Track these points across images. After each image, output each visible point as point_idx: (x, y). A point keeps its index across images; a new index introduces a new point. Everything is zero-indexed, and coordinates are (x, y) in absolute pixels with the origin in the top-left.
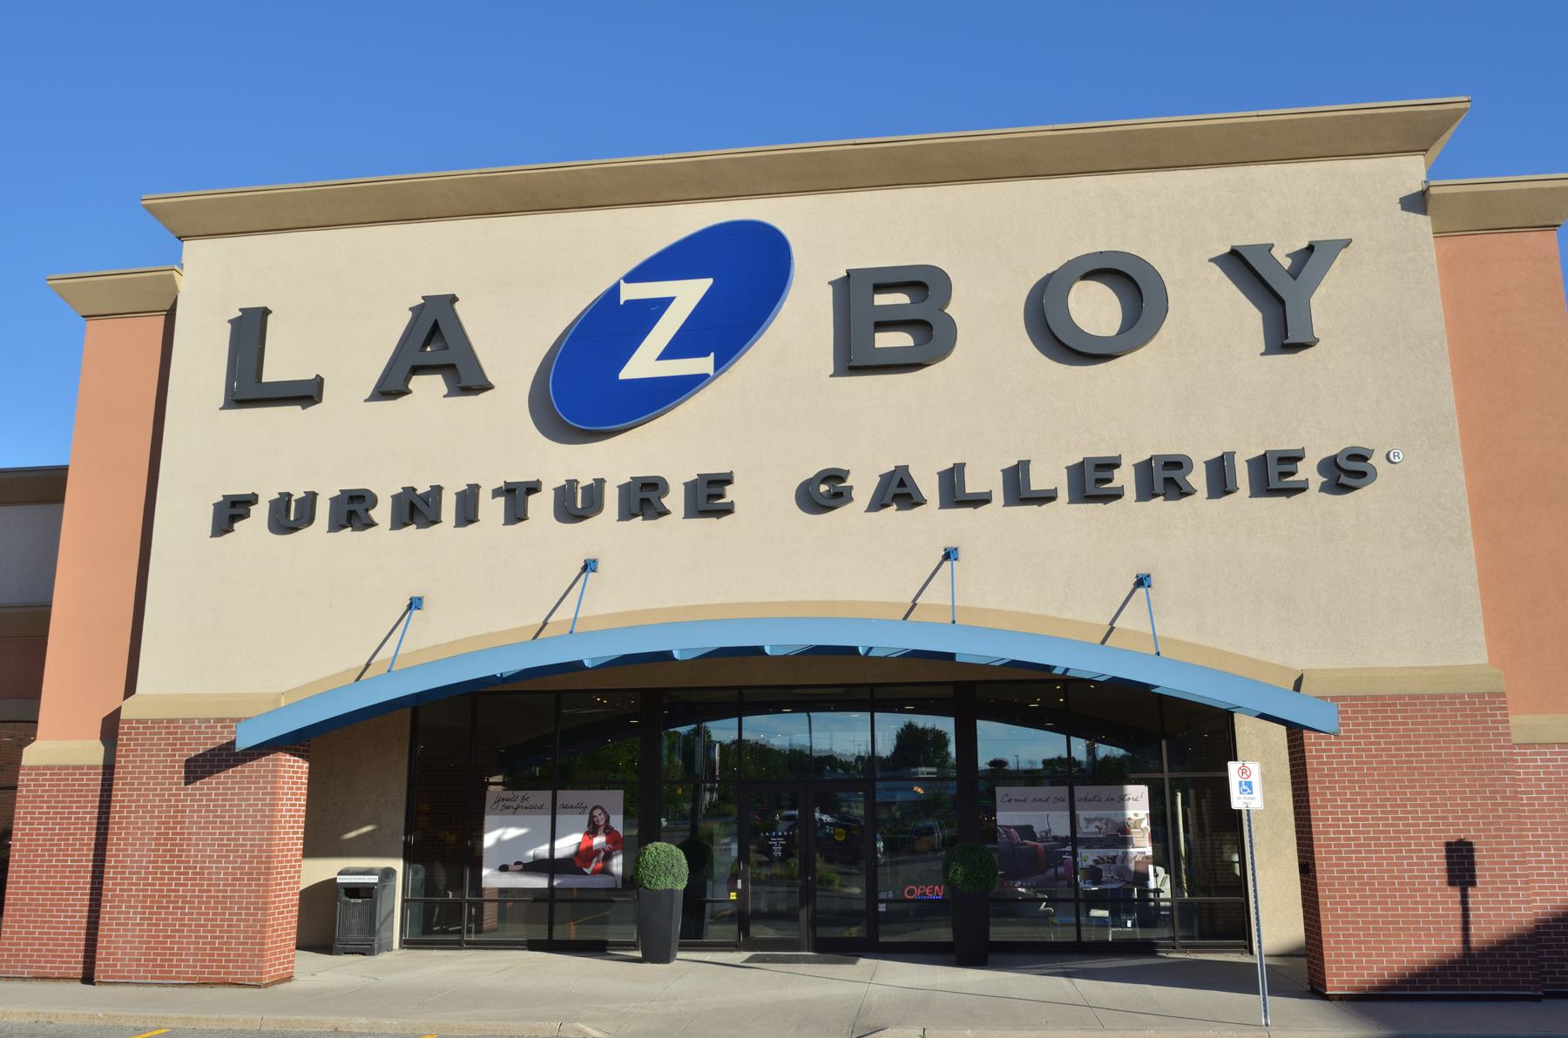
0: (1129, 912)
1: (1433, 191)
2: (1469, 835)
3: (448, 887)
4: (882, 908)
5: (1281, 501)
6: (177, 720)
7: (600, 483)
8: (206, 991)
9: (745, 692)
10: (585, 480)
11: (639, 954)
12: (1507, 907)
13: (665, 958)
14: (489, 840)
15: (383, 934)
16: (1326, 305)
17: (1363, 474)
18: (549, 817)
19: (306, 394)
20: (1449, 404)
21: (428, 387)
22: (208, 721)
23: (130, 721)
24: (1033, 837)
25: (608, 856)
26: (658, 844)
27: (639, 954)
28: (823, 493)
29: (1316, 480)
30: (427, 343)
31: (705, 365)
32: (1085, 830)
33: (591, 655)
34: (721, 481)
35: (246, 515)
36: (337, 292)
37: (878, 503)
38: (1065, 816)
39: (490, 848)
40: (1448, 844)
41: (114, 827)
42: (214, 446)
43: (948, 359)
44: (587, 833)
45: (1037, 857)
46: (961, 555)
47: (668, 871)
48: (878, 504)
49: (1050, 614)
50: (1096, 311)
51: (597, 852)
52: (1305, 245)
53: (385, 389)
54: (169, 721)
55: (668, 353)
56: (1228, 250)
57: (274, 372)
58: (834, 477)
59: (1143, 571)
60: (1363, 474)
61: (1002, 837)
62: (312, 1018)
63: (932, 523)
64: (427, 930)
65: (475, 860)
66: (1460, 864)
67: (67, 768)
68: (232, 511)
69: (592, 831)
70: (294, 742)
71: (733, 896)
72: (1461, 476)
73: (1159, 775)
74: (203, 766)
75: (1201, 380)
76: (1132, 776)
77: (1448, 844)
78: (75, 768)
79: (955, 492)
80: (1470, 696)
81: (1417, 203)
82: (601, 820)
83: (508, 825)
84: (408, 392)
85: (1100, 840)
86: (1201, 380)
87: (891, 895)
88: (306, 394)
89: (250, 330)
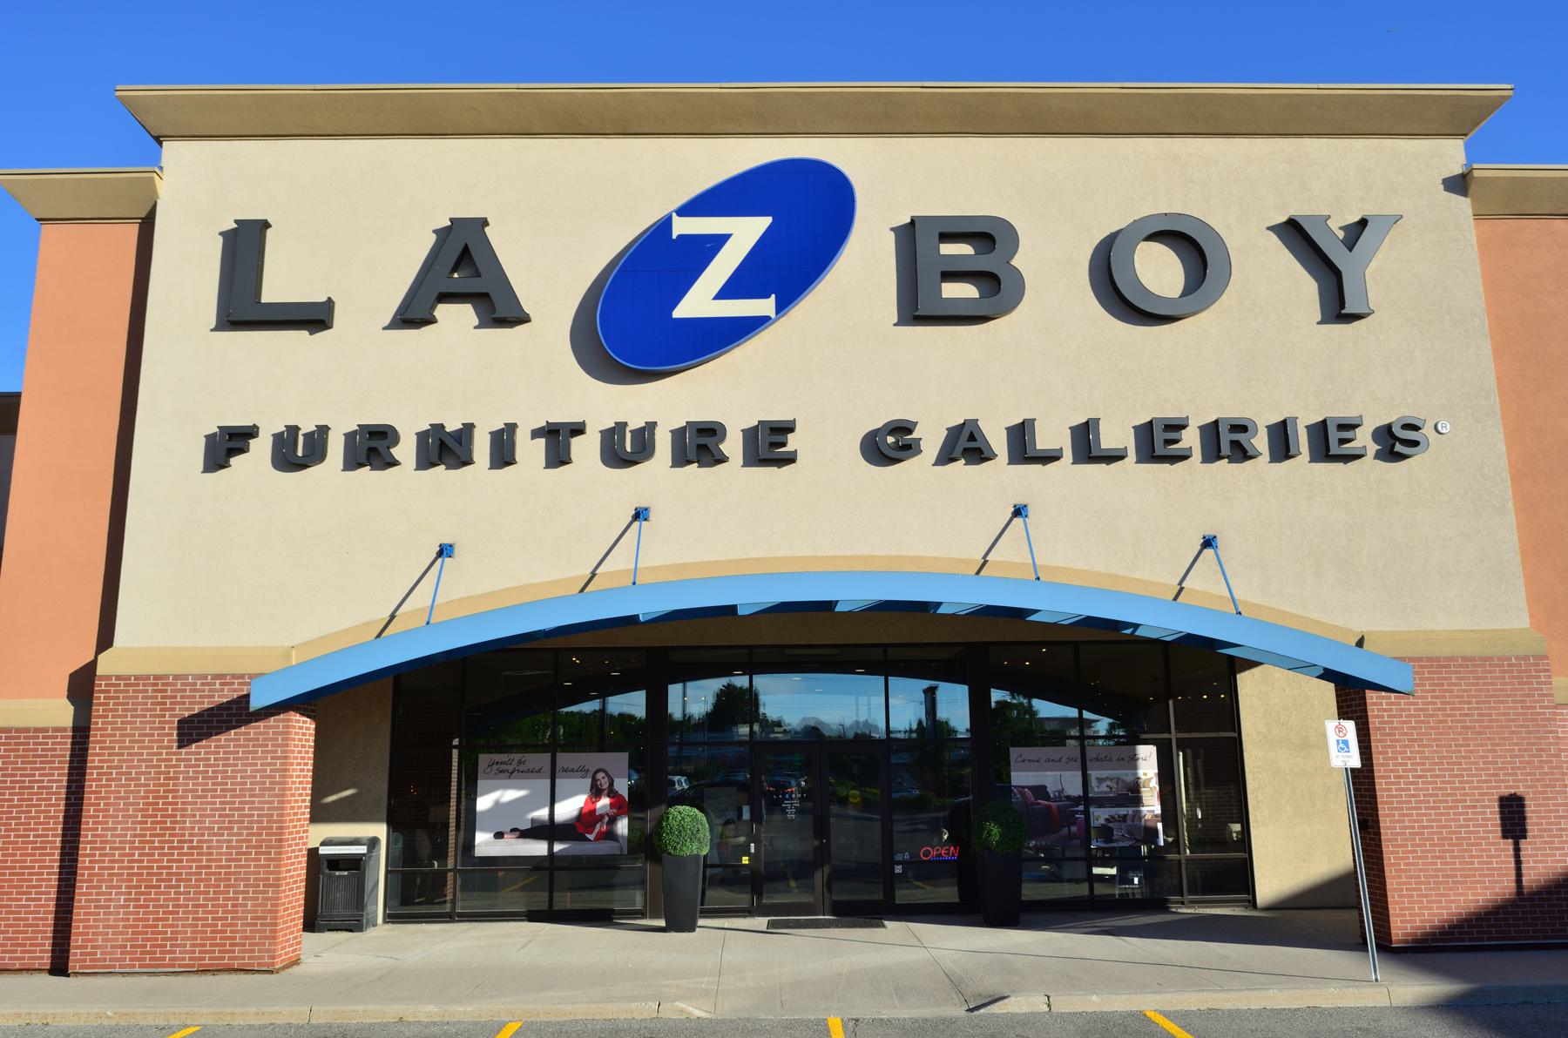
0: (1135, 869)
1: (1476, 174)
2: (1520, 791)
3: (433, 856)
4: (898, 869)
5: (772, 471)
6: (166, 677)
7: (323, 430)
8: (208, 978)
9: (890, 650)
10: (635, 423)
11: (662, 923)
12: (1550, 856)
13: (690, 927)
14: (483, 803)
15: (370, 908)
16: (1378, 275)
17: (1415, 444)
18: (548, 781)
19: (315, 318)
20: (1491, 380)
21: (456, 318)
22: (204, 677)
23: (108, 678)
24: (1046, 796)
25: (613, 820)
26: (681, 808)
27: (662, 923)
28: (889, 445)
29: (1373, 448)
30: (454, 270)
31: (766, 306)
32: (1097, 789)
33: (647, 607)
34: (783, 429)
35: (243, 450)
36: (349, 209)
37: (946, 457)
38: (1077, 776)
39: (483, 813)
40: (1502, 799)
41: (90, 798)
42: (199, 371)
43: (1015, 313)
44: (590, 798)
45: (1056, 818)
46: (652, 516)
47: (693, 837)
48: (946, 457)
49: (1120, 573)
50: (1159, 271)
51: (601, 817)
52: (1357, 219)
53: (408, 316)
54: (157, 677)
55: (726, 293)
56: (1284, 219)
57: (277, 289)
58: (902, 428)
59: (1209, 533)
60: (1415, 444)
61: (1016, 798)
62: (370, 1007)
63: (1000, 479)
64: (406, 900)
65: (469, 822)
66: (1513, 817)
67: (27, 730)
68: (227, 446)
69: (596, 792)
70: (304, 703)
71: (745, 860)
72: (1502, 448)
73: (1166, 736)
74: (194, 729)
75: (1255, 347)
76: (1144, 736)
77: (1502, 799)
78: (37, 730)
79: (1022, 446)
80: (1517, 658)
81: (1459, 184)
82: (605, 784)
83: (507, 787)
84: (433, 321)
85: (1111, 799)
86: (1255, 347)
87: (907, 856)
88: (315, 318)
89: (244, 246)
